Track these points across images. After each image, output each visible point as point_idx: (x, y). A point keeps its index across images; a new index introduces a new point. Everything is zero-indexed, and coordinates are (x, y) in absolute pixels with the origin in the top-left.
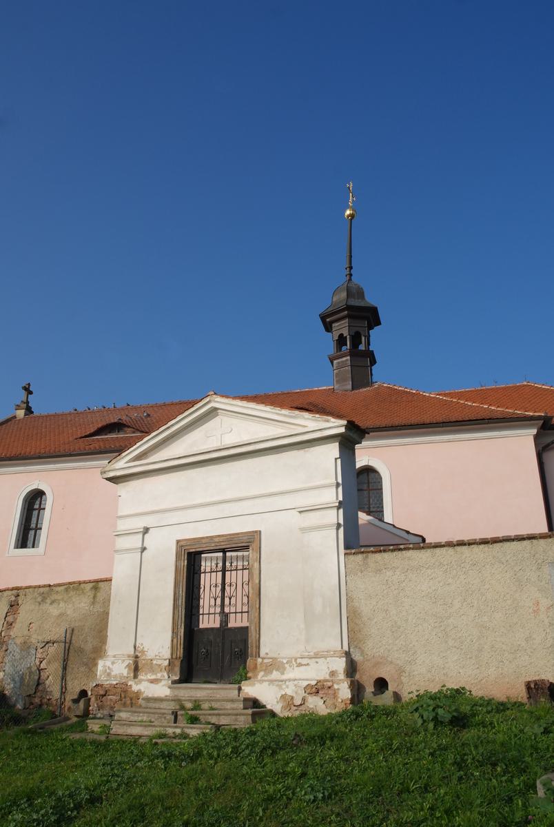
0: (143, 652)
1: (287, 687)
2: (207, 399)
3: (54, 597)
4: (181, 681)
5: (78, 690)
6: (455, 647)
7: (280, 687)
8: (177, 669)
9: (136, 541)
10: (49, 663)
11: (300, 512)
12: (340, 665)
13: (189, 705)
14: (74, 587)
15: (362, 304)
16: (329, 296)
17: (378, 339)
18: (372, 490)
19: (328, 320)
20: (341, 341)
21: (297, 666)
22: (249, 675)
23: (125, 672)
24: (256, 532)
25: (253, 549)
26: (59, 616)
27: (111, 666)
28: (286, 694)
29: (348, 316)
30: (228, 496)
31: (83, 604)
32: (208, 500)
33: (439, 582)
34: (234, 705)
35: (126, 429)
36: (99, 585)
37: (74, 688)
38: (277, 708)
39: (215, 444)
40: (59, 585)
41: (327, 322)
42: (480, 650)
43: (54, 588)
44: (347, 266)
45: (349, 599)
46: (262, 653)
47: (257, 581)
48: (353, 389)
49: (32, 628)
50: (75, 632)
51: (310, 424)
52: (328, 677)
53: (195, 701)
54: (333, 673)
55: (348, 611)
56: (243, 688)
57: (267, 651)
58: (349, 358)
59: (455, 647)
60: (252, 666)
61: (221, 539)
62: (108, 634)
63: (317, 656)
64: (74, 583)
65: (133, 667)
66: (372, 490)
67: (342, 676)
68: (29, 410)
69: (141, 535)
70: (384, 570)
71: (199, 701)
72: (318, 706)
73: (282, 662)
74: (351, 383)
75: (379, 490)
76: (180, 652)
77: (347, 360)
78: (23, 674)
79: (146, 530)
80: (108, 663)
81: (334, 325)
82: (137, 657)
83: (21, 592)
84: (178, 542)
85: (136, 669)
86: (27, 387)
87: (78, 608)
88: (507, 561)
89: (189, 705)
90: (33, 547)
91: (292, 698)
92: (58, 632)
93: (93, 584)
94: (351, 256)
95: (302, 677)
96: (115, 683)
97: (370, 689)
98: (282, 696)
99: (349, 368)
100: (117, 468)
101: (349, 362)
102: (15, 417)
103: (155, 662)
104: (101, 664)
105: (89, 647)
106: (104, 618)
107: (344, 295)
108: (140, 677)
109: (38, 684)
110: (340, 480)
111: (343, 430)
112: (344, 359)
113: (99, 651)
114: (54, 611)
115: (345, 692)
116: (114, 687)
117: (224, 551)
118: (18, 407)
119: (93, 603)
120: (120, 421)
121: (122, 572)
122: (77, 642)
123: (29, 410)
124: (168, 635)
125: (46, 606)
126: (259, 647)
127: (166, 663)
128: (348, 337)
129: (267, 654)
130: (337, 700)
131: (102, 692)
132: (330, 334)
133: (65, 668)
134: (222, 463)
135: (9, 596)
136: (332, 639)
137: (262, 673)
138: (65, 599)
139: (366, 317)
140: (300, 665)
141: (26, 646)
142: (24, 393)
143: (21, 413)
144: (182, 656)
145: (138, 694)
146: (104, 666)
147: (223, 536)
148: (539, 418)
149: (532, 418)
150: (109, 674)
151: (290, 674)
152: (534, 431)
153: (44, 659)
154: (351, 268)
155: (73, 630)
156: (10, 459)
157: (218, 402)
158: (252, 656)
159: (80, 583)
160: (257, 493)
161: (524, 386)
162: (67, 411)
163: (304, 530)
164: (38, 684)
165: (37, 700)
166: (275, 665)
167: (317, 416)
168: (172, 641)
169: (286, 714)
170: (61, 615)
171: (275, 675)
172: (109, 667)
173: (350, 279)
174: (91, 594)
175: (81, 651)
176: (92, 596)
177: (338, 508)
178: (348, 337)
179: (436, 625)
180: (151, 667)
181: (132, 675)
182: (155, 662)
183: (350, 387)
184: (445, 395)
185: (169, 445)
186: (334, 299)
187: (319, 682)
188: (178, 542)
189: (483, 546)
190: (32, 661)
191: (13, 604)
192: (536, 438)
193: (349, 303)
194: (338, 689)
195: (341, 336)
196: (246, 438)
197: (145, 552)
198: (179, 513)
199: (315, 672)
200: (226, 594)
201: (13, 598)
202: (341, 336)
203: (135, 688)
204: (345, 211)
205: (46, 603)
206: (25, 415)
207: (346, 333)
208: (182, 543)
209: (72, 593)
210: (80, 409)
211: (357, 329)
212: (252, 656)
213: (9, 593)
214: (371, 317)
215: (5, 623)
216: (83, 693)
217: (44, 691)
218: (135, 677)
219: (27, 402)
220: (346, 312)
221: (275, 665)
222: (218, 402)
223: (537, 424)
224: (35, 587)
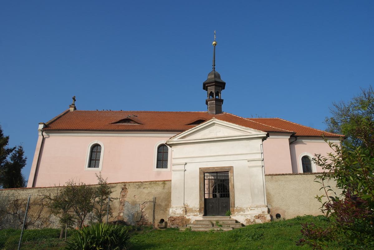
0: (187, 206)
1: (248, 216)
2: (212, 120)
5: (160, 219)
7: (245, 216)
9: (182, 167)
10: (146, 210)
11: (248, 161)
12: (266, 210)
15: (220, 81)
17: (223, 94)
19: (206, 85)
20: (211, 94)
21: (250, 210)
22: (232, 213)
23: (182, 213)
24: (232, 167)
25: (230, 172)
26: (148, 193)
27: (175, 211)
28: (247, 219)
29: (215, 85)
30: (220, 154)
31: (159, 189)
32: (212, 155)
33: (297, 185)
34: (232, 222)
35: (131, 122)
37: (158, 218)
38: (245, 223)
41: (205, 87)
43: (144, 183)
44: (213, 64)
45: (267, 190)
46: (236, 206)
47: (233, 183)
48: (216, 114)
49: (136, 197)
50: (156, 199)
51: (253, 132)
52: (261, 213)
53: (217, 221)
54: (263, 212)
55: (267, 193)
56: (231, 217)
57: (238, 206)
58: (214, 101)
60: (232, 210)
61: (218, 168)
62: (172, 199)
63: (257, 207)
65: (185, 211)
67: (266, 213)
68: (75, 109)
71: (218, 221)
72: (259, 221)
73: (244, 209)
76: (203, 206)
77: (214, 102)
78: (134, 214)
79: (186, 164)
80: (174, 209)
81: (208, 87)
83: (127, 184)
84: (200, 168)
87: (157, 190)
91: (250, 220)
92: (151, 198)
93: (163, 182)
94: (215, 61)
95: (253, 213)
96: (178, 216)
97: (275, 217)
98: (246, 219)
100: (174, 140)
102: (69, 111)
103: (193, 209)
104: (171, 210)
107: (213, 76)
108: (187, 214)
112: (213, 102)
114: (146, 191)
115: (268, 218)
116: (178, 217)
118: (71, 106)
122: (158, 202)
123: (75, 109)
125: (141, 189)
126: (234, 204)
127: (198, 209)
128: (214, 93)
129: (238, 206)
130: (266, 220)
131: (173, 219)
132: (207, 91)
134: (222, 142)
136: (262, 201)
138: (150, 187)
139: (220, 85)
140: (251, 210)
141: (134, 204)
142: (73, 100)
143: (72, 109)
144: (204, 207)
145: (189, 220)
146: (172, 211)
147: (219, 167)
148: (291, 133)
149: (289, 133)
150: (175, 213)
151: (247, 213)
152: (289, 137)
153: (143, 208)
154: (215, 65)
155: (156, 198)
156: (100, 131)
157: (216, 121)
158: (232, 207)
159: (156, 181)
160: (230, 153)
163: (250, 167)
166: (241, 210)
167: (256, 130)
168: (200, 202)
169: (248, 225)
171: (241, 213)
172: (174, 211)
174: (162, 185)
175: (160, 205)
176: (163, 186)
178: (214, 93)
180: (192, 210)
181: (185, 213)
182: (193, 209)
183: (215, 113)
184: (249, 119)
185: (195, 134)
186: (209, 77)
188: (200, 168)
189: (311, 175)
191: (123, 188)
192: (289, 139)
194: (266, 217)
195: (211, 92)
196: (226, 135)
197: (186, 171)
198: (181, 159)
199: (257, 212)
200: (205, 187)
202: (211, 92)
203: (187, 218)
204: (213, 41)
205: (141, 188)
206: (74, 110)
207: (213, 91)
208: (202, 169)
209: (153, 185)
211: (218, 90)
212: (232, 207)
213: (121, 184)
214: (220, 85)
215: (121, 195)
216: (162, 221)
217: (144, 219)
220: (214, 83)
221: (241, 210)
222: (216, 121)
223: (289, 135)
224: (134, 182)
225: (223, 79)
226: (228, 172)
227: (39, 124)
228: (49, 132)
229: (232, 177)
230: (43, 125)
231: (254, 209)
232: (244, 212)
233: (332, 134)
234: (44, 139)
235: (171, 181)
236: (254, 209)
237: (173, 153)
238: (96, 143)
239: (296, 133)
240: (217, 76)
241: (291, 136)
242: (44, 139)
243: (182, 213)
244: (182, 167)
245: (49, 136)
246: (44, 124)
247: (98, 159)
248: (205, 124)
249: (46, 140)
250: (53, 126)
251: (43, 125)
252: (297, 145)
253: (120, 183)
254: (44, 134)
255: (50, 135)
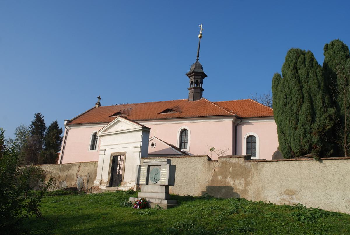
0: (103, 179)
3: (87, 165)
4: (109, 186)
5: (90, 187)
8: (109, 183)
9: (103, 152)
13: (107, 191)
14: (91, 163)
16: (189, 68)
29: (194, 75)
36: (96, 162)
39: (119, 129)
40: (89, 162)
46: (124, 181)
48: (194, 100)
58: (193, 89)
64: (91, 162)
69: (104, 151)
74: (193, 98)
79: (105, 150)
80: (96, 182)
82: (102, 180)
85: (101, 183)
86: (99, 97)
87: (91, 168)
89: (107, 191)
90: (95, 149)
92: (86, 174)
94: (199, 52)
99: (193, 93)
101: (193, 91)
102: (95, 107)
105: (93, 178)
106: (96, 171)
109: (83, 186)
110: (142, 141)
111: (142, 129)
113: (95, 179)
114: (87, 168)
116: (96, 187)
118: (96, 104)
119: (94, 167)
120: (120, 112)
121: (100, 160)
122: (91, 176)
123: (100, 105)
124: (108, 175)
133: (88, 182)
135: (79, 164)
137: (123, 185)
143: (97, 106)
149: (233, 116)
152: (232, 120)
159: (92, 162)
161: (248, 100)
162: (110, 105)
163: (134, 152)
164: (83, 186)
165: (83, 190)
170: (88, 170)
171: (125, 185)
173: (198, 61)
174: (94, 165)
175: (91, 178)
177: (141, 148)
183: (193, 100)
187: (131, 187)
188: (111, 153)
190: (81, 181)
193: (194, 71)
196: (126, 128)
201: (80, 165)
208: (112, 154)
209: (91, 164)
210: (114, 105)
213: (79, 163)
218: (101, 185)
219: (99, 102)
220: (193, 74)
227: (65, 121)
228: (70, 126)
230: (67, 121)
232: (127, 185)
234: (67, 131)
237: (101, 142)
242: (67, 131)
245: (71, 129)
246: (68, 120)
247: (187, 135)
248: (116, 120)
249: (69, 131)
250: (74, 122)
251: (67, 121)
252: (244, 126)
254: (67, 127)
255: (71, 128)
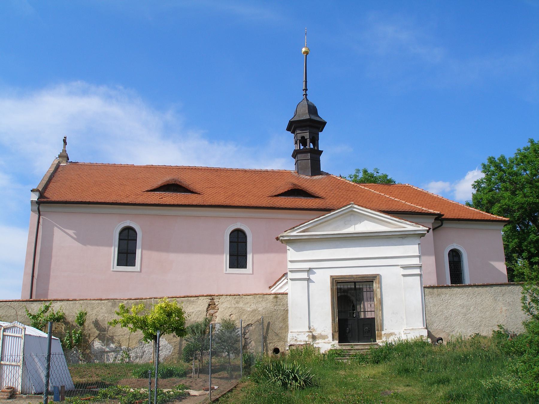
6: (471, 325)
18: (238, 245)
25: (376, 283)
42: (480, 326)
59: (471, 325)
66: (238, 245)
70: (441, 295)
75: (246, 242)
84: (331, 276)
88: (491, 293)
93: (275, 295)
117: (355, 283)
158: (378, 330)
172: (295, 337)
179: (463, 317)
188: (331, 276)
191: (210, 303)
195: (303, 137)
202: (303, 137)
203: (315, 345)
214: (320, 125)
225: (323, 114)
226: (373, 281)
229: (378, 290)
231: (410, 333)
233: (498, 217)
235: (287, 294)
236: (410, 333)
238: (128, 225)
239: (443, 215)
240: (312, 110)
241: (436, 219)
243: (307, 339)
244: (304, 275)
253: (203, 296)
